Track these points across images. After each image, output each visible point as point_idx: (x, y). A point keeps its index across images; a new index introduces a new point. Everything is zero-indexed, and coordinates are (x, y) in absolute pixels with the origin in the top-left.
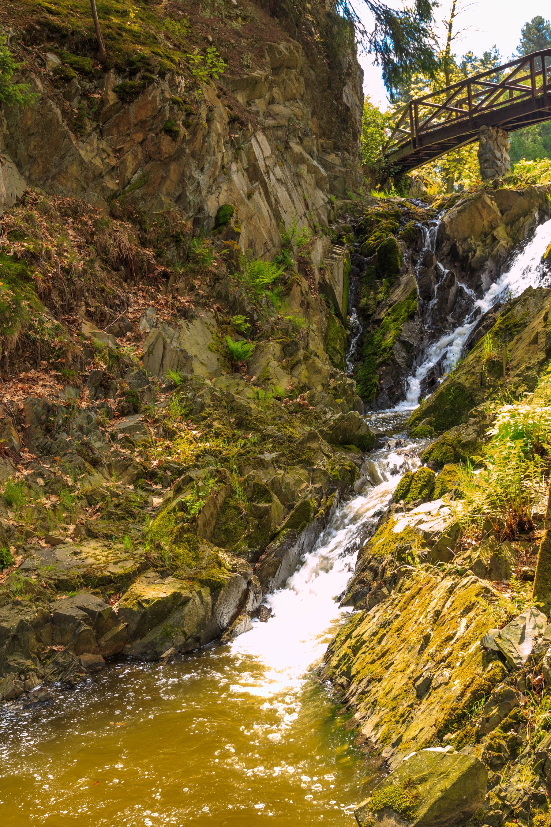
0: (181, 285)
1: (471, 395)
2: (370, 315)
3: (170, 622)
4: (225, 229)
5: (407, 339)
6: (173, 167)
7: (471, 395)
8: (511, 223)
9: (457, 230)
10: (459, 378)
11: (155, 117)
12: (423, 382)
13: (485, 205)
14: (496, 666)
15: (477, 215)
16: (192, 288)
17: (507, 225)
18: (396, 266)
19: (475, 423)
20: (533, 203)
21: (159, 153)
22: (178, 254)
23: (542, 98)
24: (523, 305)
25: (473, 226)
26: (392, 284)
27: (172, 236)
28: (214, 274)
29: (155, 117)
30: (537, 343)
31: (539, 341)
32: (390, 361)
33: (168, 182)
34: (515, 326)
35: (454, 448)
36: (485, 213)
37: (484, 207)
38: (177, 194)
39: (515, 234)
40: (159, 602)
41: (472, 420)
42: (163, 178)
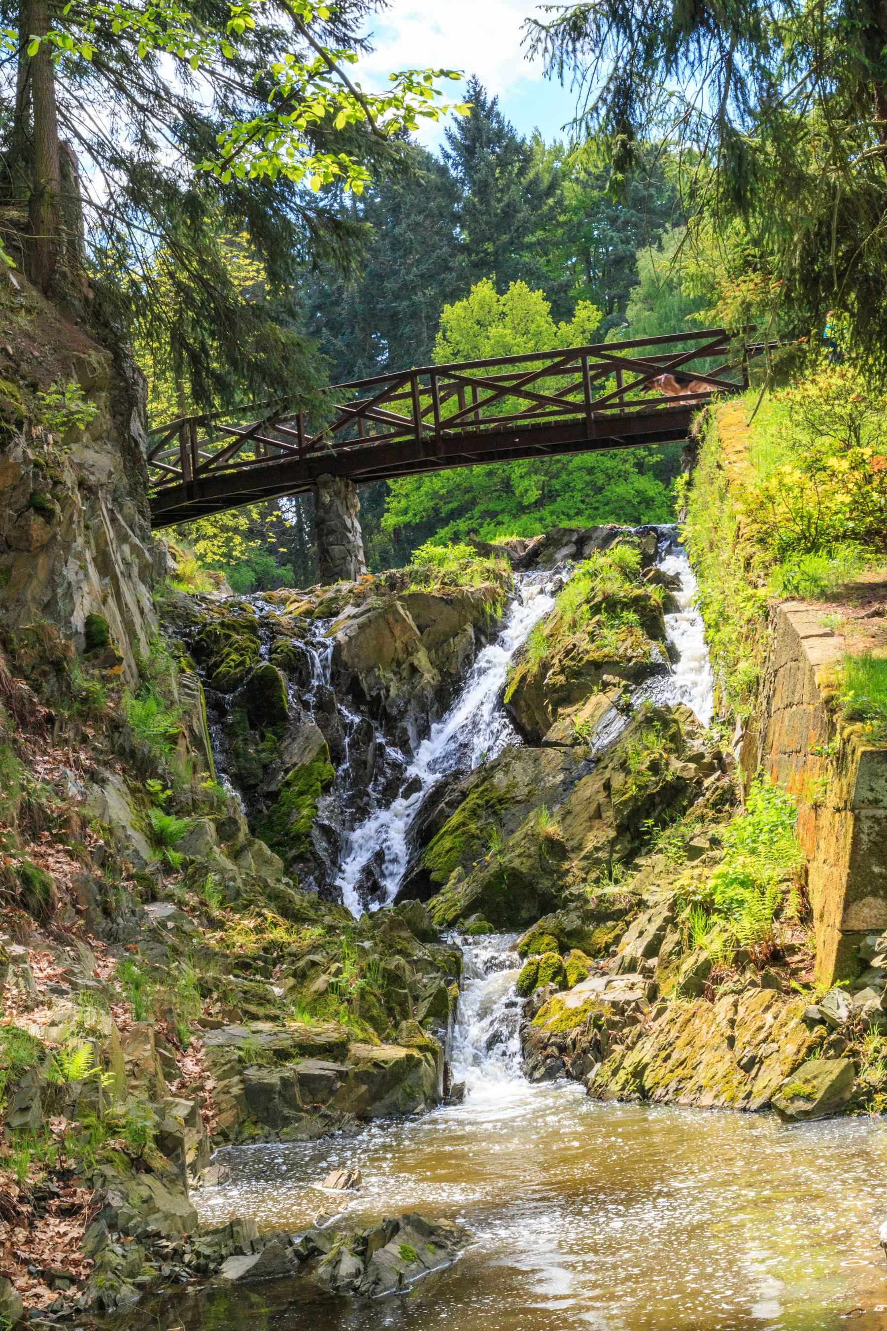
0: (69, 734)
1: (531, 884)
2: (255, 786)
3: (407, 1083)
4: (102, 652)
5: (326, 822)
6: (42, 560)
7: (531, 884)
8: (436, 645)
9: (358, 656)
10: (511, 861)
11: (14, 488)
12: (359, 887)
13: (400, 620)
14: (820, 1030)
15: (386, 632)
16: (84, 739)
17: (429, 649)
18: (283, 708)
19: (576, 908)
20: (465, 616)
21: (27, 540)
22: (60, 688)
23: (433, 440)
24: (506, 772)
25: (381, 649)
26: (280, 738)
27: (52, 663)
28: (113, 720)
29: (14, 488)
30: (600, 817)
31: (604, 815)
32: (309, 856)
33: (35, 582)
34: (500, 801)
35: (557, 937)
36: (397, 631)
37: (397, 621)
38: (46, 599)
39: (443, 663)
40: (397, 1063)
41: (572, 905)
42: (30, 576)
